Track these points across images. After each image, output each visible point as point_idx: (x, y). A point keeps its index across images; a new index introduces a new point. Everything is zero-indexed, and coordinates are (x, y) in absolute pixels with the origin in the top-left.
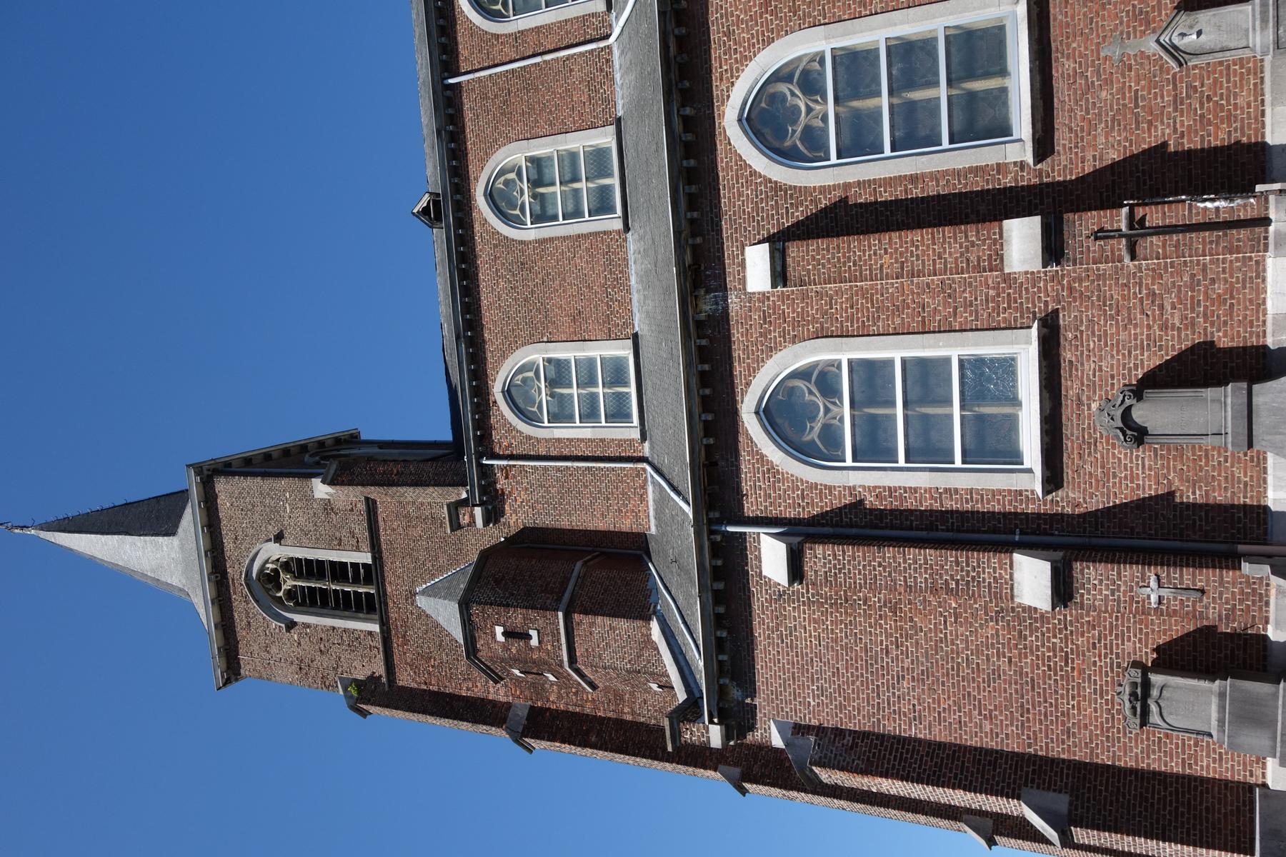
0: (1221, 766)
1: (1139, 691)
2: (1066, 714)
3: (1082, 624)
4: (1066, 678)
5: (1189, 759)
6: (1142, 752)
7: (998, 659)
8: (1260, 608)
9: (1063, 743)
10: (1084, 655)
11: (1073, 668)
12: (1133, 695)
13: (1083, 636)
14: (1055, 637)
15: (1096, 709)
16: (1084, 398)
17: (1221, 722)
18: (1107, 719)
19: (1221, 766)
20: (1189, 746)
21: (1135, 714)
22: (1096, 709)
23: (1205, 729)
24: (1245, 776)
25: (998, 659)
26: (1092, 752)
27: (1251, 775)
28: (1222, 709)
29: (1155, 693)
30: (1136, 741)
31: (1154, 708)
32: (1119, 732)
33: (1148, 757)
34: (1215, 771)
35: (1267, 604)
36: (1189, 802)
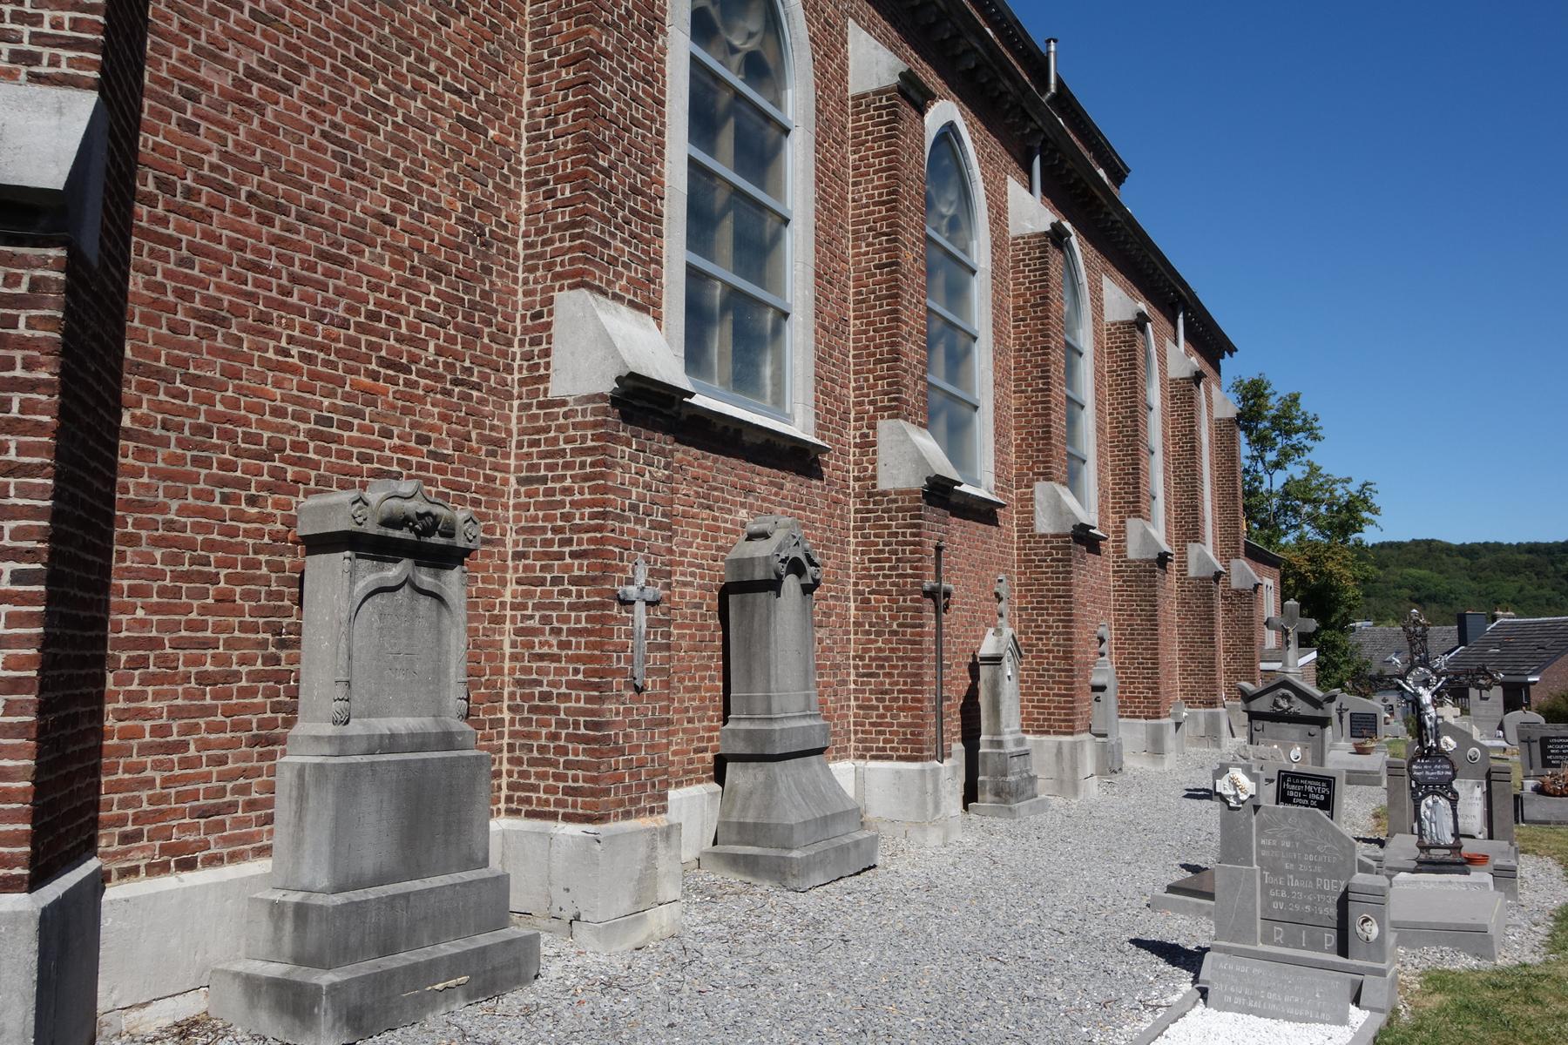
0: (145, 750)
1: (436, 539)
2: (262, 325)
3: (462, 422)
4: (349, 352)
5: (163, 661)
6: (170, 525)
7: (388, 191)
8: (621, 803)
9: (182, 295)
10: (406, 411)
11: (375, 376)
12: (429, 524)
13: (444, 418)
14: (440, 352)
15: (277, 412)
16: (750, 500)
17: (390, 743)
18: (256, 440)
19: (145, 750)
20: (199, 661)
21: (388, 522)
22: (281, 413)
23: (357, 705)
24: (122, 821)
25: (388, 191)
26: (160, 374)
27: (126, 838)
28: (420, 742)
29: (425, 578)
30: (204, 512)
31: (394, 572)
32: (224, 465)
33: (156, 542)
34: (126, 734)
35: (627, 815)
36: (902, 659)
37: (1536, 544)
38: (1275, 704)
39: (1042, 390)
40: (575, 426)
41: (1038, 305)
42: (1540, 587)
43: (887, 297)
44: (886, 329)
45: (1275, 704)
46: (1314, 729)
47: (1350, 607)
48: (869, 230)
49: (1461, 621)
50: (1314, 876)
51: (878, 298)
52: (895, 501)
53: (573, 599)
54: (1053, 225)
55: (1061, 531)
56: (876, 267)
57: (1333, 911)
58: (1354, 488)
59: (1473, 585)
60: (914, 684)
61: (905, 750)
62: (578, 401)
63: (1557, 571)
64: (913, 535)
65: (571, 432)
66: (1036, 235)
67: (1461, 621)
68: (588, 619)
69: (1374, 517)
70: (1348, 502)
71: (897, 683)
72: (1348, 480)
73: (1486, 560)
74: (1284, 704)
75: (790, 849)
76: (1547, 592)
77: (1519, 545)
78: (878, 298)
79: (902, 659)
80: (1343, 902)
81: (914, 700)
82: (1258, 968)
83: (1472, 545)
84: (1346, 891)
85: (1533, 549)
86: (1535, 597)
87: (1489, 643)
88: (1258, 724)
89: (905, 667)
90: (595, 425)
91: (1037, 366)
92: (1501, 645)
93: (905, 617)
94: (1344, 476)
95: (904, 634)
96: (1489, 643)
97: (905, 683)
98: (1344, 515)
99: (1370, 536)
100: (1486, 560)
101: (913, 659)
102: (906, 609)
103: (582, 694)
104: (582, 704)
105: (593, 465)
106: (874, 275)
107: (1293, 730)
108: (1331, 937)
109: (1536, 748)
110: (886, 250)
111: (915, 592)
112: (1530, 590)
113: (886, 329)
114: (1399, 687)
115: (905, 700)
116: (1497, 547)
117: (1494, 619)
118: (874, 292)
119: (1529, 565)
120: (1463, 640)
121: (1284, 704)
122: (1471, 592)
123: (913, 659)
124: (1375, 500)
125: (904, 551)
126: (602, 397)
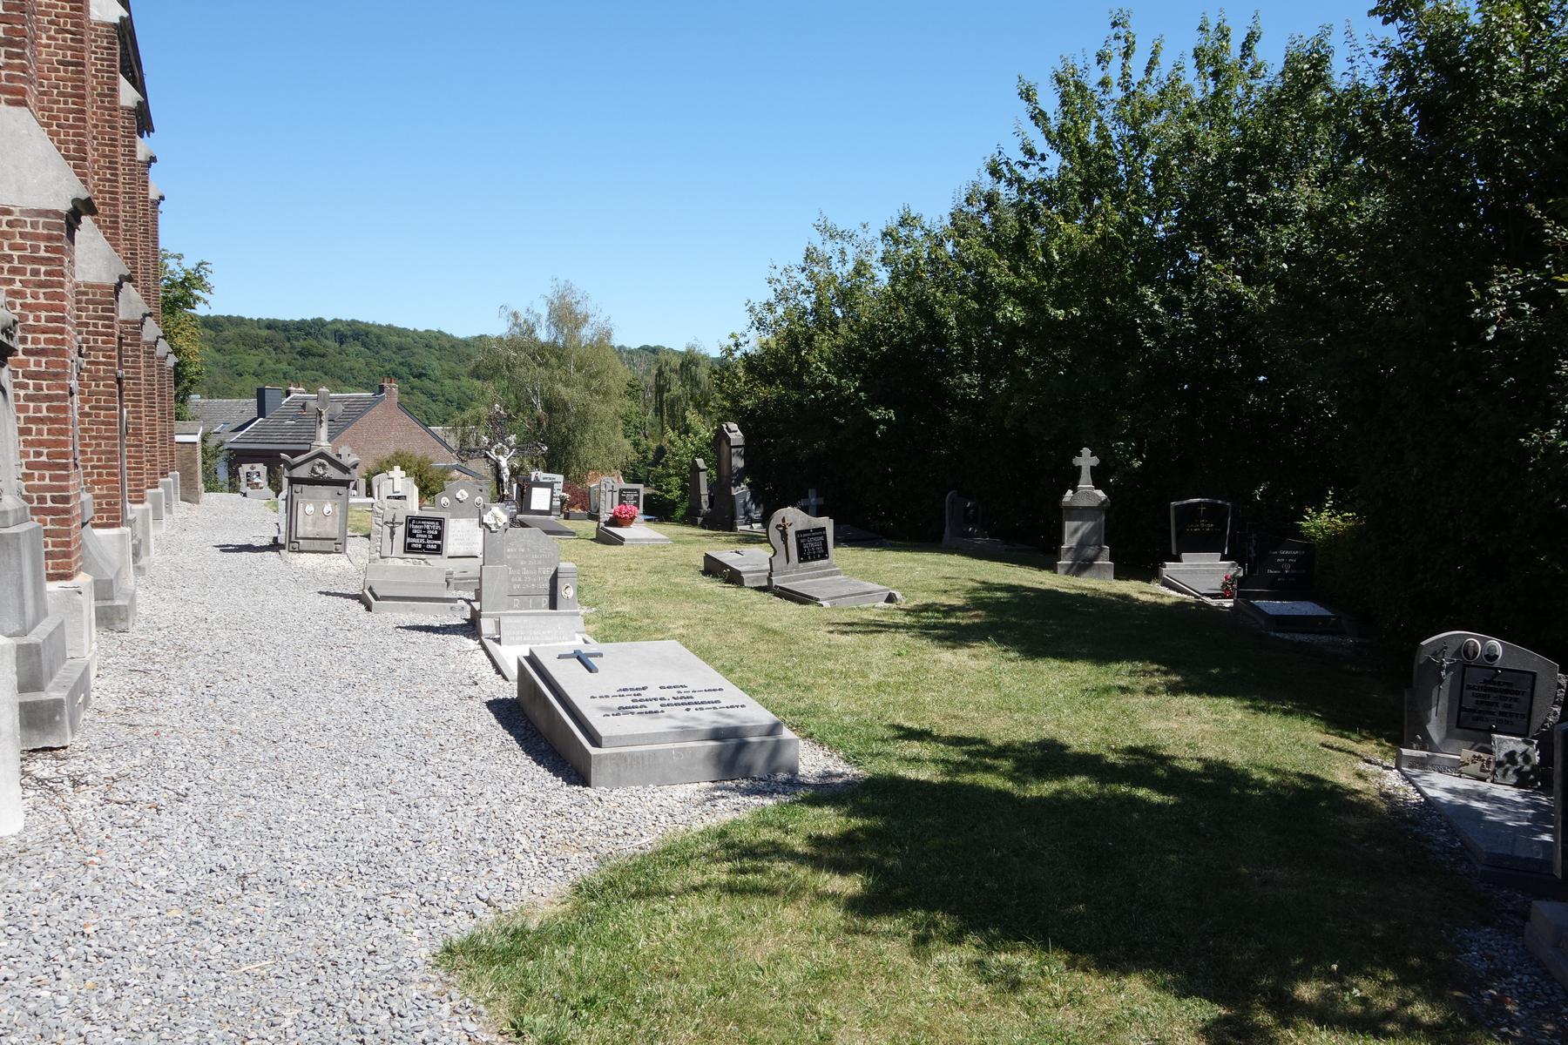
36: (95, 438)
37: (275, 321)
38: (313, 471)
39: (109, 180)
40: (22, 235)
41: (106, 96)
42: (278, 361)
43: (72, 96)
44: (71, 127)
45: (313, 471)
46: (342, 489)
47: (192, 382)
48: (50, 22)
49: (261, 395)
50: (537, 566)
51: (60, 94)
52: (85, 293)
53: (31, 391)
54: (122, 18)
55: (130, 318)
56: (59, 62)
57: (547, 586)
58: (189, 264)
59: (218, 356)
60: (108, 460)
61: (101, 518)
62: (23, 212)
63: (293, 347)
64: (104, 326)
65: (19, 241)
66: (104, 24)
67: (261, 395)
68: (48, 409)
69: (205, 296)
70: (186, 279)
71: (91, 460)
72: (180, 257)
73: (230, 332)
74: (320, 471)
75: (112, 599)
76: (284, 366)
77: (259, 320)
78: (60, 94)
79: (95, 438)
80: (554, 579)
81: (108, 474)
82: (526, 620)
83: (216, 318)
84: (556, 572)
85: (271, 325)
86: (274, 371)
87: (285, 416)
88: (297, 487)
89: (99, 445)
90: (49, 238)
91: (105, 156)
92: (296, 417)
93: (98, 401)
94: (176, 252)
95: (97, 416)
96: (285, 416)
97: (99, 460)
98: (178, 292)
99: (201, 310)
100: (230, 332)
101: (108, 438)
102: (99, 393)
103: (47, 474)
104: (47, 481)
105: (47, 273)
106: (58, 70)
107: (326, 491)
108: (546, 600)
109: (616, 495)
110: (71, 48)
111: (110, 378)
112: (270, 364)
113: (71, 127)
114: (486, 456)
115: (99, 475)
116: (240, 321)
117: (288, 393)
118: (57, 87)
119: (268, 341)
120: (262, 412)
121: (320, 471)
122: (216, 363)
123: (108, 438)
124: (209, 279)
125: (96, 341)
126: (57, 214)
